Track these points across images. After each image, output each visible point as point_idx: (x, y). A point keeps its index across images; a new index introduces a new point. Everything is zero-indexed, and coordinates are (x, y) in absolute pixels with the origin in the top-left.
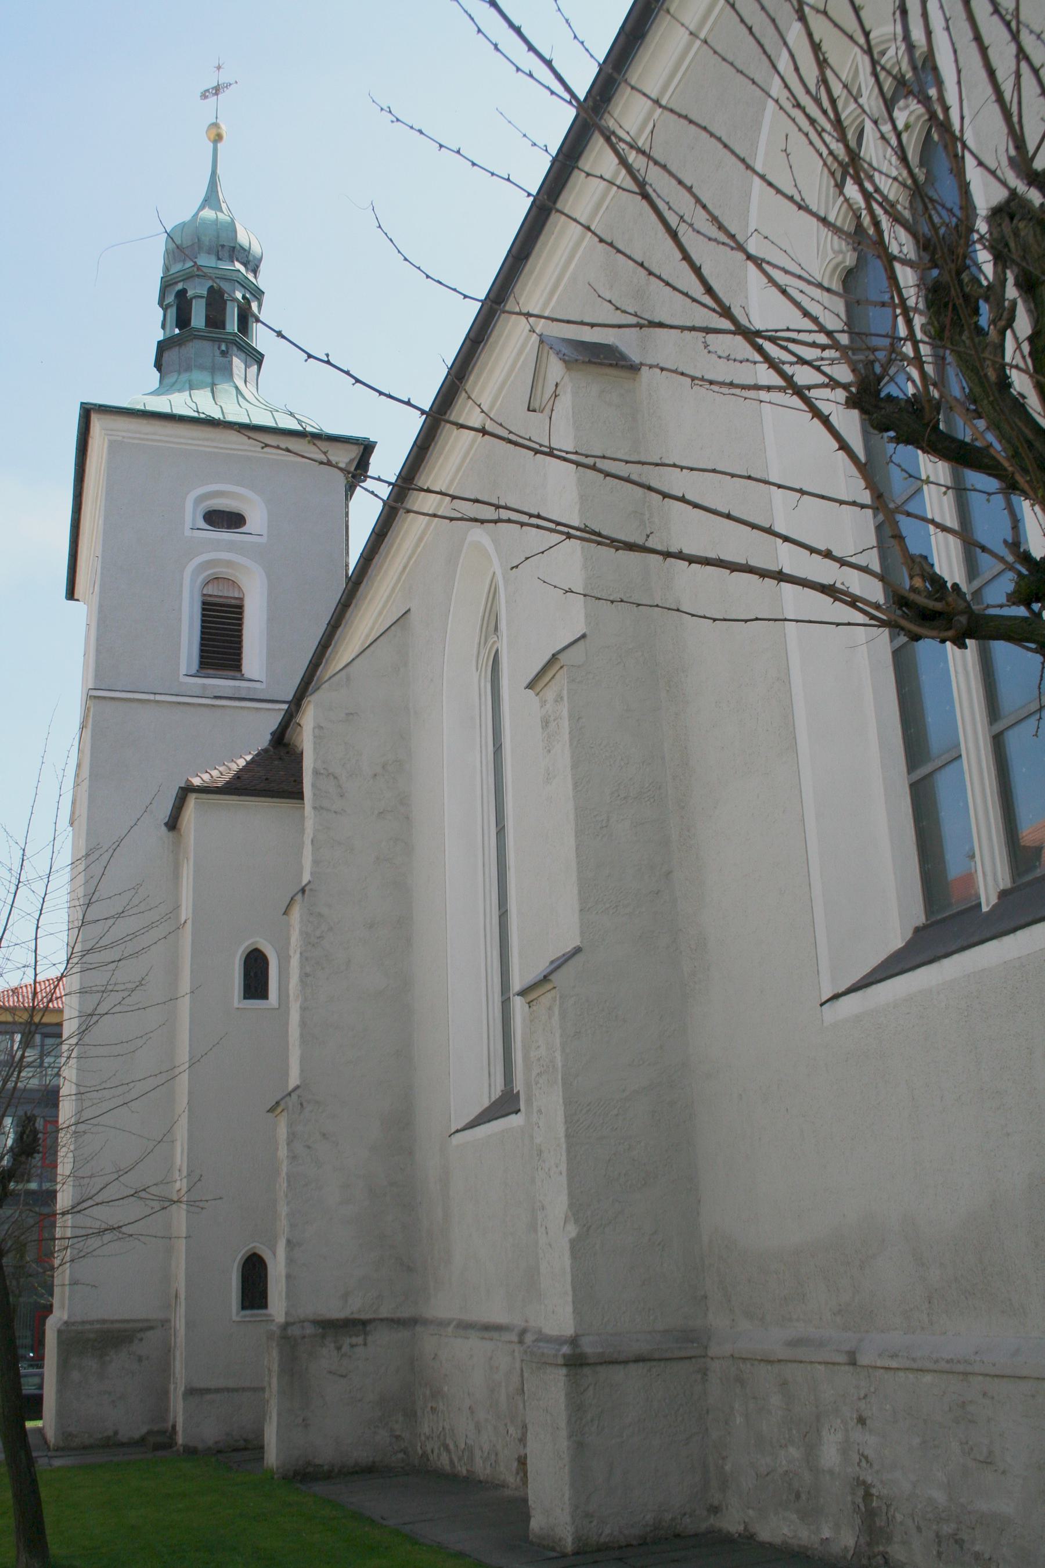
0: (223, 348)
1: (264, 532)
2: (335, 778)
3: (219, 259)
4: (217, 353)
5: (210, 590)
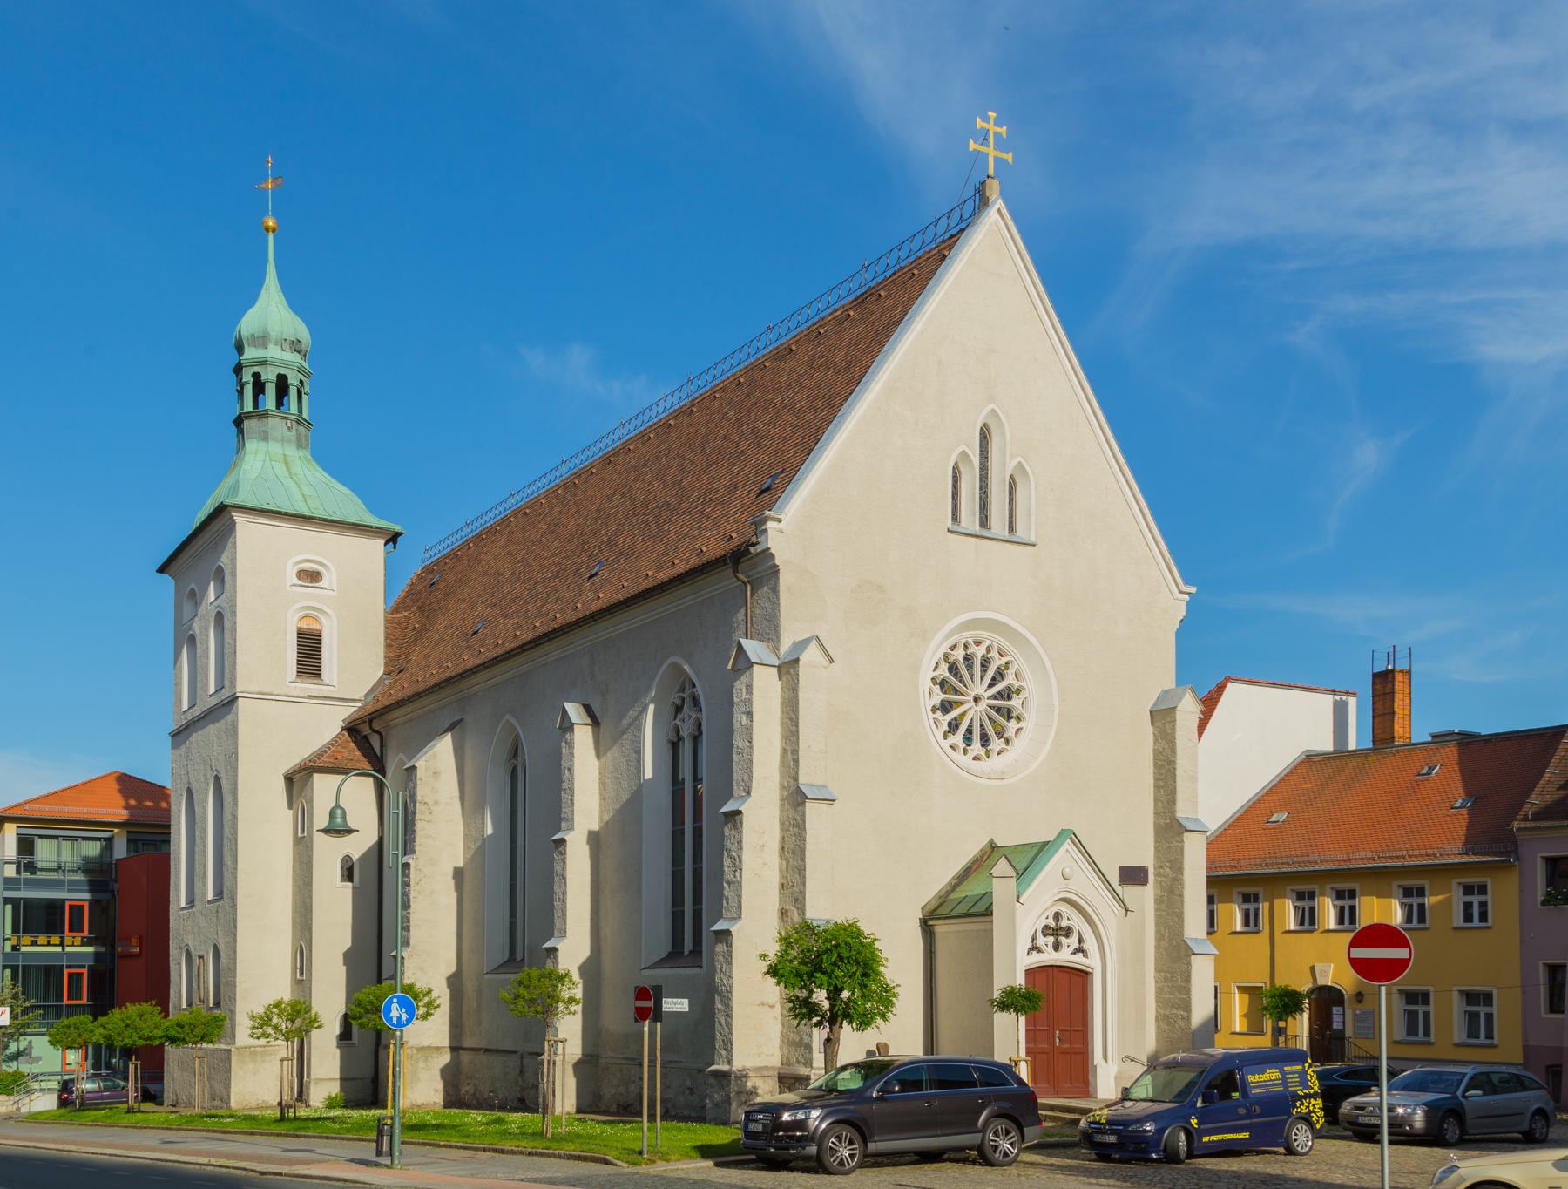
1: (335, 587)
2: (428, 805)
5: (304, 625)
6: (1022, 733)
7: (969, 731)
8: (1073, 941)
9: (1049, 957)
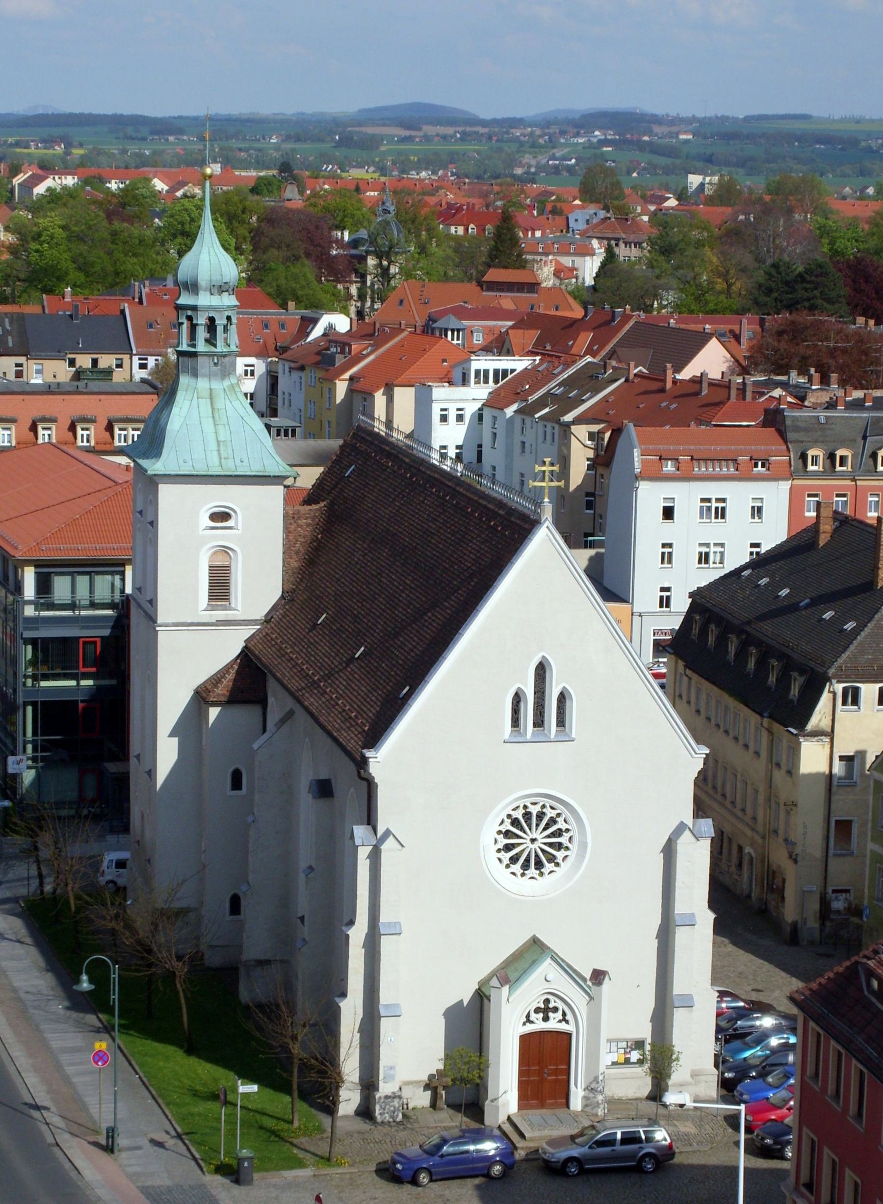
0: (216, 361)
3: (212, 294)
4: (212, 364)
6: (568, 858)
7: (527, 860)
8: (559, 1015)
9: (539, 1025)
